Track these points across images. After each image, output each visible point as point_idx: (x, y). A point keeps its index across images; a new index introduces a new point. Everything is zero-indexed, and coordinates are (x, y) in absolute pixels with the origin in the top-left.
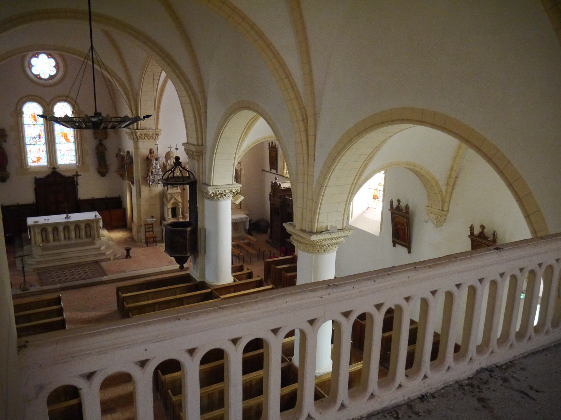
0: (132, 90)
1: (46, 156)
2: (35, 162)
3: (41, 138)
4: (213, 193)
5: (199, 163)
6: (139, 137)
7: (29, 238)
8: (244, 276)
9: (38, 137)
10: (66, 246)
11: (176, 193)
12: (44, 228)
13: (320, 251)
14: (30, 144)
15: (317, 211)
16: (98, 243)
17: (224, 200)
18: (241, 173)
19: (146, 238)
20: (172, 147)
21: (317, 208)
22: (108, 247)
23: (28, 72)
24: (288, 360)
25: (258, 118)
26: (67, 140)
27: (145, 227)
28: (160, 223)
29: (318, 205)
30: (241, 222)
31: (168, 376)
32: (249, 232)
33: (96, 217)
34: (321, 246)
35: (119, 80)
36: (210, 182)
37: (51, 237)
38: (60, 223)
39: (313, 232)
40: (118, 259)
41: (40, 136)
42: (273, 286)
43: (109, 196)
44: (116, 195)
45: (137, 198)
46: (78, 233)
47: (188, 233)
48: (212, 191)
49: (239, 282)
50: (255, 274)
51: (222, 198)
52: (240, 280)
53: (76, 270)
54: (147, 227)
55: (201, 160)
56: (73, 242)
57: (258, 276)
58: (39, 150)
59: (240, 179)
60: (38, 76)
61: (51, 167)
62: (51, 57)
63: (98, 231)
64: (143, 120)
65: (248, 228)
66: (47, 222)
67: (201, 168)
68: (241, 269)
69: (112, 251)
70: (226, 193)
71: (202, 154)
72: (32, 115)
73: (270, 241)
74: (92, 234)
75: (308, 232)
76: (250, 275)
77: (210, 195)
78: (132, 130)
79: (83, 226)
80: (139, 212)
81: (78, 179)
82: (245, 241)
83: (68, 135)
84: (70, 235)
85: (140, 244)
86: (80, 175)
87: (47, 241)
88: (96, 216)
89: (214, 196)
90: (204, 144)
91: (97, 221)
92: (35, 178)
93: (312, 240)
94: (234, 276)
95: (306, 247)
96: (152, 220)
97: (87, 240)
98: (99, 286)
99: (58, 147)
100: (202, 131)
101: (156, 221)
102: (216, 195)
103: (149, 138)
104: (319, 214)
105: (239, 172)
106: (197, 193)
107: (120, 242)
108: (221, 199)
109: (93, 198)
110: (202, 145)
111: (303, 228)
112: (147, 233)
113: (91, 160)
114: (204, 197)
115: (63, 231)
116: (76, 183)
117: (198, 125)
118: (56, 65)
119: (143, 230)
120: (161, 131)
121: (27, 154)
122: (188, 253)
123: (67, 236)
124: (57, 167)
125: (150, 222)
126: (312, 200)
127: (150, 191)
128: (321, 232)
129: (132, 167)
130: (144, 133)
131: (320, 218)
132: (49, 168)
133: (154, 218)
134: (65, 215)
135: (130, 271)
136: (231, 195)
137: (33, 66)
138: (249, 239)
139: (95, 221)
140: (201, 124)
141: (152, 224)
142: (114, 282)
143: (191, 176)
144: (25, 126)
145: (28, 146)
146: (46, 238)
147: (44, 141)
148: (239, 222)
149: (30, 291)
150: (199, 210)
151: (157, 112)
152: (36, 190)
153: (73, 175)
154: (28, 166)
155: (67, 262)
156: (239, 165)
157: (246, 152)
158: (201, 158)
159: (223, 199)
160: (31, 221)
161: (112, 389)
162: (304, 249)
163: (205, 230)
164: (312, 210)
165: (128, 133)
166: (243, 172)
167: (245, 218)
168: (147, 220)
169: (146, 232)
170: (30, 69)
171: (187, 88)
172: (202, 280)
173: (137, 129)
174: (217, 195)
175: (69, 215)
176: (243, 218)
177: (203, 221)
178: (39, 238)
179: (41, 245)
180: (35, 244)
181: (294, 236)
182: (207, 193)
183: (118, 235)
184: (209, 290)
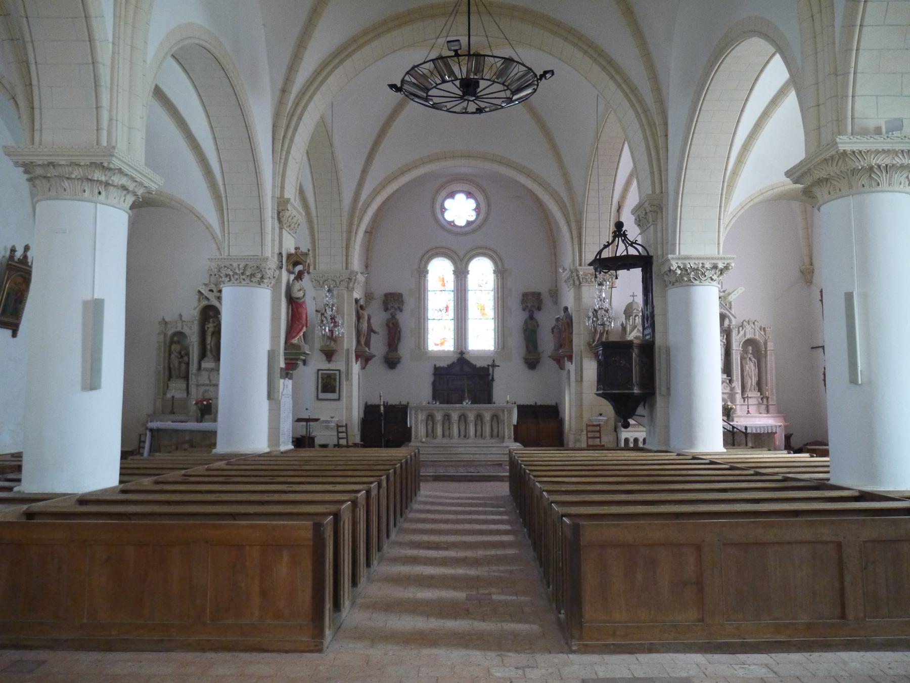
2: (437, 345)
4: (679, 267)
6: (583, 278)
7: (409, 426)
9: (445, 309)
14: (434, 319)
18: (766, 348)
20: (636, 296)
23: (439, 216)
28: (613, 428)
35: (554, 195)
41: (447, 308)
43: (539, 403)
44: (550, 402)
46: (479, 428)
48: (677, 263)
54: (590, 429)
55: (659, 220)
58: (445, 328)
60: (452, 223)
62: (470, 198)
67: (659, 234)
71: (661, 209)
81: (494, 372)
86: (498, 366)
87: (433, 437)
100: (660, 171)
101: (607, 421)
105: (763, 347)
108: (697, 282)
113: (517, 342)
115: (458, 421)
116: (490, 378)
118: (476, 207)
122: (635, 388)
129: (571, 331)
131: (857, 107)
137: (446, 209)
139: (505, 410)
141: (599, 425)
144: (430, 293)
145: (430, 322)
146: (433, 432)
152: (434, 384)
153: (489, 365)
157: (746, 208)
158: (659, 216)
163: (668, 350)
166: (770, 346)
170: (443, 213)
174: (688, 274)
179: (424, 440)
180: (416, 437)
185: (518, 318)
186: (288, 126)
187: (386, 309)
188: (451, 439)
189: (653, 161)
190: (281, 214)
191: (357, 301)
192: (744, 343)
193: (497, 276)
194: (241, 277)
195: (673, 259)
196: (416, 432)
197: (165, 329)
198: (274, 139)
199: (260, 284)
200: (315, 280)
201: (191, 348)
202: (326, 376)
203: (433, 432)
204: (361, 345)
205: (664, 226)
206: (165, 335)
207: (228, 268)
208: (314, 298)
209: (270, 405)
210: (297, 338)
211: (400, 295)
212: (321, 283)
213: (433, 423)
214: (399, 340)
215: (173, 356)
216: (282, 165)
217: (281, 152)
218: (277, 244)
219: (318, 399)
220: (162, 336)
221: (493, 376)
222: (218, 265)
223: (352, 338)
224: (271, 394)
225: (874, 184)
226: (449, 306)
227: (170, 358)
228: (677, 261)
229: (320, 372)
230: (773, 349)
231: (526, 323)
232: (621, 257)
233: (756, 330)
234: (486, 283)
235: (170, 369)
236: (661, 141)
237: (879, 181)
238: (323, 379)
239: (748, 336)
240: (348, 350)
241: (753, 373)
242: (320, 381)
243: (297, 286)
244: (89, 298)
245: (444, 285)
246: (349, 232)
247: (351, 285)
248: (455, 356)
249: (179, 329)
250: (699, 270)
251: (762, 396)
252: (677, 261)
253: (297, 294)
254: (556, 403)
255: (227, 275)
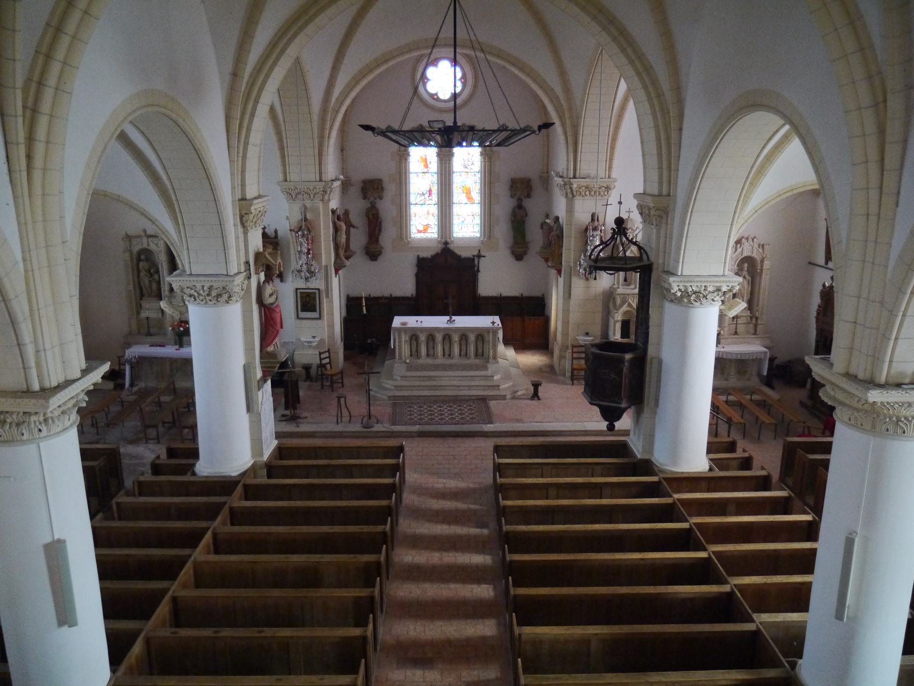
0: (570, 108)
1: (436, 223)
2: (419, 232)
3: (433, 194)
4: (680, 290)
5: (658, 232)
8: (735, 463)
10: (444, 368)
11: (633, 294)
12: (414, 335)
13: (891, 432)
14: (416, 204)
15: (891, 331)
16: (492, 367)
17: (701, 306)
18: (762, 266)
19: (573, 370)
21: (893, 325)
22: (507, 377)
24: (786, 665)
25: (789, 138)
26: (470, 198)
27: (572, 350)
29: (896, 316)
30: (753, 360)
31: (528, 630)
32: (768, 382)
33: (493, 325)
34: (894, 419)
35: (549, 91)
36: (677, 267)
37: (423, 350)
38: (438, 329)
39: (877, 381)
40: (519, 398)
41: (430, 191)
42: (791, 493)
43: (526, 294)
44: (536, 293)
45: (564, 298)
46: (464, 348)
47: (626, 364)
48: (678, 286)
49: (718, 473)
50: (755, 463)
51: (699, 302)
52: (721, 468)
53: (451, 407)
54: (575, 350)
55: (664, 226)
56: (454, 361)
57: (763, 468)
58: (428, 213)
59: (761, 278)
61: (443, 240)
63: (495, 347)
64: (537, 132)
65: (765, 373)
66: (419, 325)
67: (662, 240)
68: (731, 447)
69: (511, 383)
70: (707, 292)
71: (667, 214)
72: (421, 157)
73: (809, 403)
74: (485, 353)
75: (861, 381)
76: (746, 463)
77: (674, 294)
78: (565, 180)
79: (472, 337)
80: (566, 323)
82: (755, 397)
83: (471, 189)
84: (452, 350)
85: (561, 378)
86: (484, 256)
88: (493, 323)
89: (682, 296)
90: (671, 194)
91: (495, 331)
92: (418, 256)
93: (871, 400)
94: (711, 460)
95: (856, 418)
96: (585, 338)
97: (477, 361)
98: (476, 438)
99: (456, 209)
100: (669, 182)
102: (686, 294)
103: (593, 193)
104: (896, 339)
105: (759, 265)
106: (651, 291)
107: (527, 371)
109: (501, 295)
110: (669, 195)
111: (853, 371)
112: (575, 362)
113: (503, 231)
114: (665, 297)
115: (442, 342)
116: (476, 268)
117: (664, 158)
119: (568, 355)
120: (614, 181)
121: (410, 219)
122: (624, 402)
123: (447, 352)
124: (451, 241)
125: (582, 343)
126: (882, 303)
127: (588, 287)
128: (899, 385)
130: (585, 184)
132: (439, 242)
133: (590, 337)
134: (448, 318)
135: (531, 422)
136: (718, 297)
138: (765, 395)
139: (491, 331)
140: (669, 153)
142: (500, 437)
143: (645, 257)
144: (411, 175)
146: (417, 351)
147: (436, 200)
148: (748, 360)
149: (373, 429)
150: (653, 322)
151: (611, 147)
152: (417, 275)
153: (474, 256)
154: (410, 238)
155: (439, 393)
156: (761, 250)
158: (664, 221)
159: (701, 304)
160: (398, 321)
161: (440, 623)
162: (850, 420)
163: (660, 362)
164: (878, 329)
165: (559, 185)
166: (767, 264)
167: (761, 353)
168: (578, 338)
169: (573, 358)
171: (648, 82)
172: (646, 457)
173: (575, 177)
175: (454, 318)
176: (757, 353)
177: (659, 344)
178: (406, 350)
179: (408, 361)
180: (400, 358)
181: (828, 387)
182: (668, 290)
183: (532, 359)
184: (655, 479)
185: (505, 204)
186: (243, 114)
187: (365, 197)
188: (435, 359)
189: (661, 239)
190: (244, 218)
191: (333, 212)
192: (740, 261)
193: (484, 158)
194: (207, 298)
195: (674, 281)
196: (400, 354)
197: (130, 247)
198: (228, 131)
199: (228, 303)
200: (287, 193)
201: (160, 266)
202: (305, 295)
203: (417, 351)
204: (341, 259)
205: (668, 232)
206: (131, 252)
207: (191, 289)
208: (287, 218)
209: (250, 417)
210: (272, 346)
211: (380, 181)
212: (294, 196)
213: (417, 343)
214: (380, 231)
215: (142, 274)
216: (240, 159)
217: (238, 147)
218: (242, 253)
219: (298, 317)
220: (128, 254)
221: (478, 267)
222: (180, 286)
223: (330, 254)
224: (250, 407)
225: (899, 431)
226: (432, 189)
227: (139, 276)
228: (678, 284)
229: (299, 291)
230: (769, 267)
231: (514, 210)
232: (621, 257)
233: (754, 248)
234: (473, 164)
235: (141, 288)
236: (674, 135)
237: (905, 429)
238: (302, 298)
239: (745, 254)
240: (326, 267)
241: (746, 291)
242: (299, 300)
243: (269, 289)
244: (48, 540)
245: (426, 166)
246: (321, 137)
247: (326, 197)
248: (439, 246)
249: (145, 246)
250: (701, 293)
251: (751, 315)
252: (678, 284)
253: (269, 300)
254: (543, 295)
255: (191, 296)
